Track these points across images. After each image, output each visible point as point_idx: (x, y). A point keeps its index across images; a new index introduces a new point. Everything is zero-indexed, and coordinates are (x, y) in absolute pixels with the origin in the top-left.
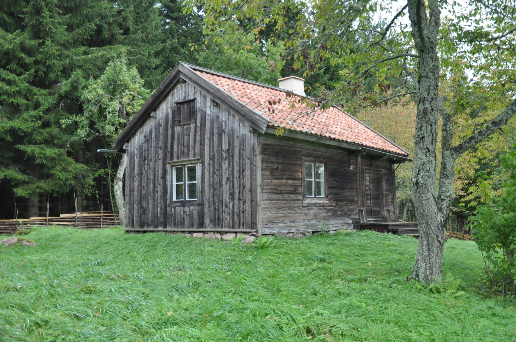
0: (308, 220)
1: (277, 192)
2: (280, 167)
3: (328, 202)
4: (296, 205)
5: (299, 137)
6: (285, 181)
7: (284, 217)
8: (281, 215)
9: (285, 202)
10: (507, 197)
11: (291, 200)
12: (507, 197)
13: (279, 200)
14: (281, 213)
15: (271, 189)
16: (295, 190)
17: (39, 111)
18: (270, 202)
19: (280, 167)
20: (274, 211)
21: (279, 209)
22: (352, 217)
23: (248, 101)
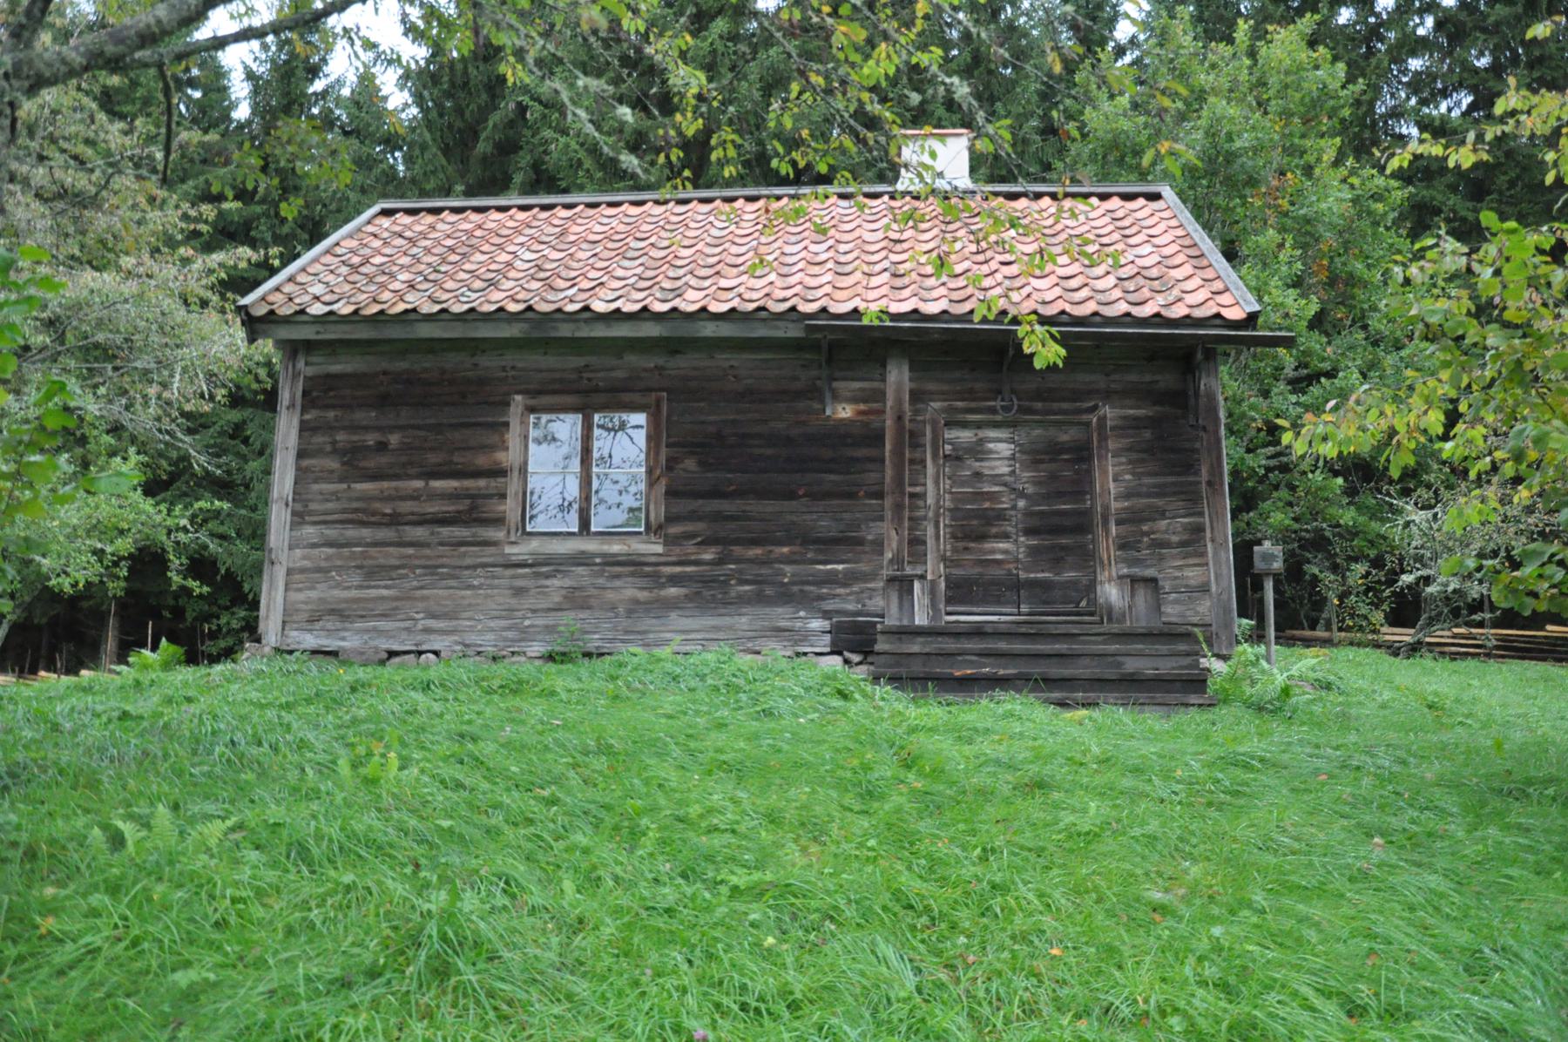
0: (534, 611)
1: (373, 519)
2: (394, 439)
3: (659, 549)
4: (468, 561)
5: (709, 330)
6: (419, 484)
7: (397, 599)
8: (385, 592)
9: (411, 551)
10: (20, 366)
11: (442, 544)
12: (20, 366)
13: (375, 544)
14: (386, 587)
15: (344, 511)
16: (473, 508)
17: (1090, 718)
18: (330, 551)
19: (394, 439)
20: (356, 579)
21: (373, 573)
22: (829, 605)
23: (1075, 134)
